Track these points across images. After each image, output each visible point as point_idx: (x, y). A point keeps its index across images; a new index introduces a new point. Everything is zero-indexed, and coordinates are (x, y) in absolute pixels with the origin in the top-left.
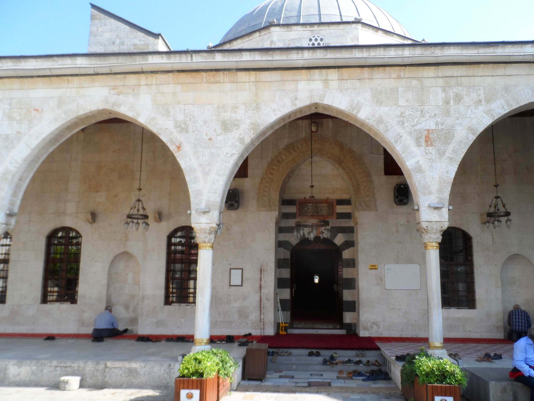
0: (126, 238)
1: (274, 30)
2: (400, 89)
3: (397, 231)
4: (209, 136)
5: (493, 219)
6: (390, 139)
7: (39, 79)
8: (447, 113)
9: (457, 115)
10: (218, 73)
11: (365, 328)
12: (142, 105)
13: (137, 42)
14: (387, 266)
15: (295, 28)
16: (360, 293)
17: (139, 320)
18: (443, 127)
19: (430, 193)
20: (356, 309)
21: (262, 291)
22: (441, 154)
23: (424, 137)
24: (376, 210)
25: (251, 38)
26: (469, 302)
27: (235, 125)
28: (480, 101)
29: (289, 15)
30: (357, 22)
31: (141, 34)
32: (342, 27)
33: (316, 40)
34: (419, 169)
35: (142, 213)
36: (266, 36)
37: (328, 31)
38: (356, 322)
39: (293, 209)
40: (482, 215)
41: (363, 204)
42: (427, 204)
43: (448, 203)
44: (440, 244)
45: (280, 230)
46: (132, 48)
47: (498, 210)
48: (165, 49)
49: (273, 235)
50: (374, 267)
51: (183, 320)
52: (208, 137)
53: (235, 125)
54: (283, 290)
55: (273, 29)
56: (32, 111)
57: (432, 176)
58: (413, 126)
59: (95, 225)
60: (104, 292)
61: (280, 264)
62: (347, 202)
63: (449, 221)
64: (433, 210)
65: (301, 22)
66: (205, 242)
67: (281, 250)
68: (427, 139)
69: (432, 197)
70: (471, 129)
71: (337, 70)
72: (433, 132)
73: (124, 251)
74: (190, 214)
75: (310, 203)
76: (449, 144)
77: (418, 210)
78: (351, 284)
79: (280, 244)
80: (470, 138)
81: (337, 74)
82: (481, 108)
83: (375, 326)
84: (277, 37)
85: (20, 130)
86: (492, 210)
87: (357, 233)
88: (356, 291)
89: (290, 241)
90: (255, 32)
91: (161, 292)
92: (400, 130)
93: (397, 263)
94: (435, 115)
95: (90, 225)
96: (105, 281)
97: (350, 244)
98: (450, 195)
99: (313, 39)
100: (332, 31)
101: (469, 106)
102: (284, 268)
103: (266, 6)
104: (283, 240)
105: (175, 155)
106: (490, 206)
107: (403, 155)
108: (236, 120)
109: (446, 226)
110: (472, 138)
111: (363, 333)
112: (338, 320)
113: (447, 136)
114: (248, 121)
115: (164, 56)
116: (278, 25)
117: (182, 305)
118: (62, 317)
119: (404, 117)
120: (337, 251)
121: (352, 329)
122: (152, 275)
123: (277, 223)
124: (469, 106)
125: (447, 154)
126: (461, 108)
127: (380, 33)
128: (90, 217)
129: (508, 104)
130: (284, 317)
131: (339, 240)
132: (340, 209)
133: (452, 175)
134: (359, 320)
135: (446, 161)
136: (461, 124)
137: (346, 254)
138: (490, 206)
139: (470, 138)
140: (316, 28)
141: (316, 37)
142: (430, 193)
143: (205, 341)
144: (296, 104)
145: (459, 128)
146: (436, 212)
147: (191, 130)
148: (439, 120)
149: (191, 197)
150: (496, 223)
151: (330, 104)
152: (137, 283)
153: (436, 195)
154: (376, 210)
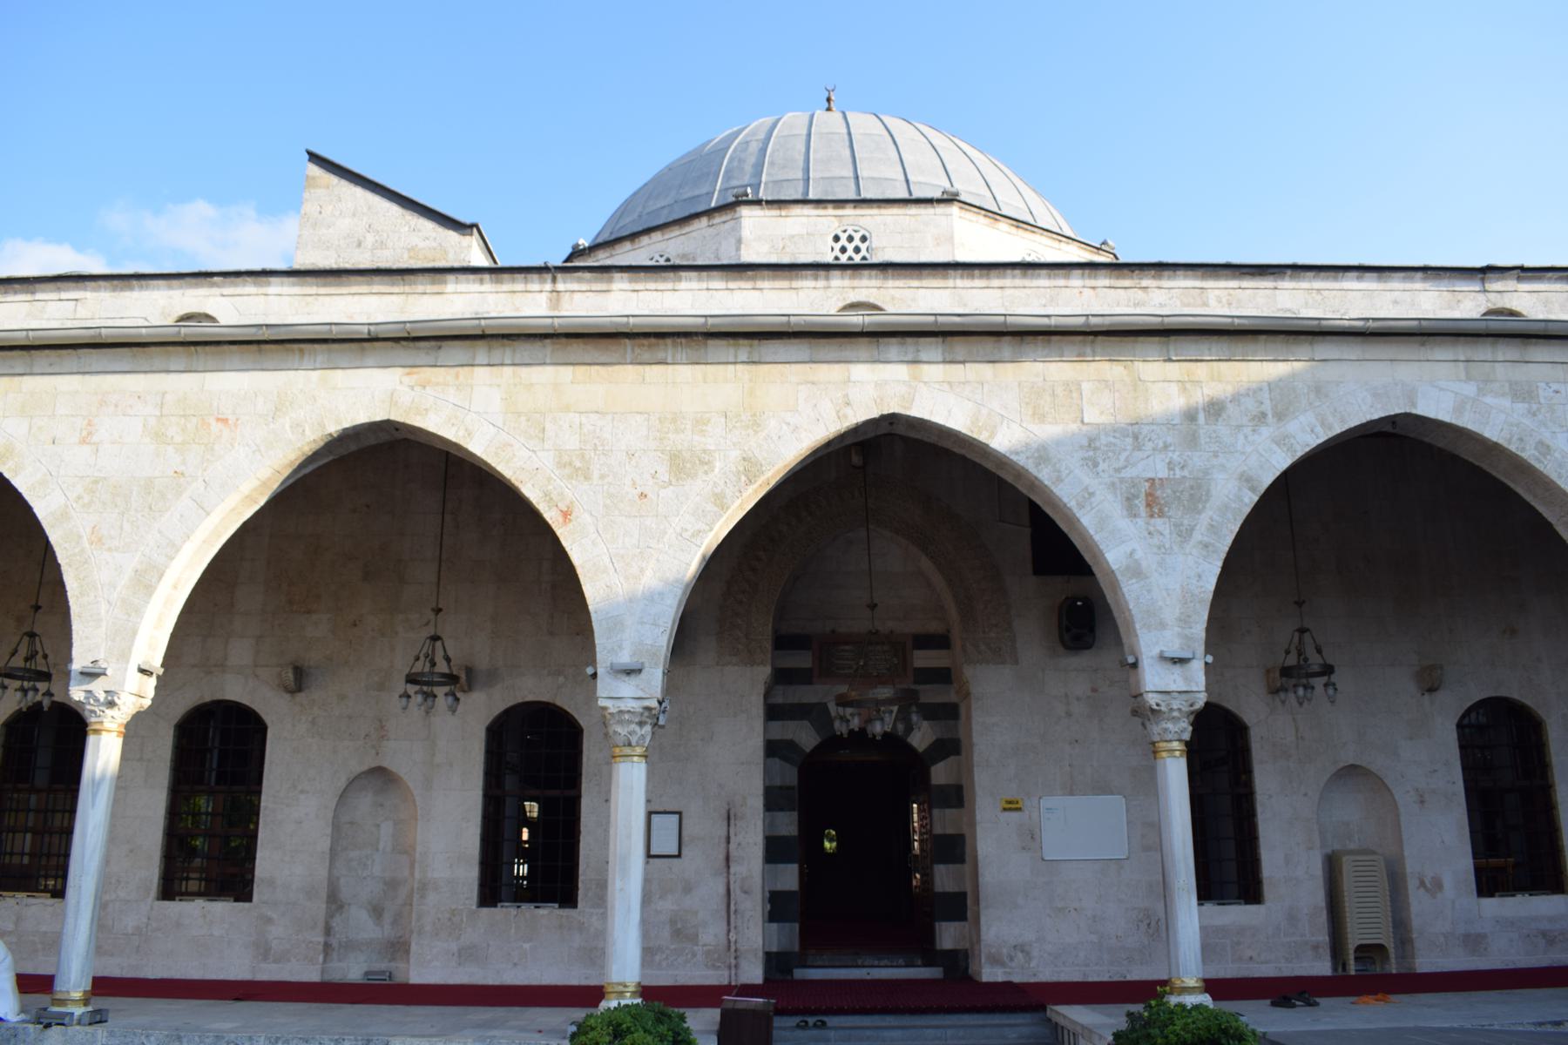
0: (381, 730)
1: (750, 217)
2: (1085, 386)
3: (1069, 714)
4: (643, 485)
5: (1293, 681)
6: (1065, 500)
7: (234, 348)
8: (1192, 441)
9: (1215, 447)
10: (661, 341)
11: (996, 961)
12: (466, 409)
13: (415, 240)
14: (1046, 802)
15: (797, 210)
16: (981, 871)
17: (414, 948)
18: (1186, 473)
19: (1163, 625)
20: (969, 914)
21: (732, 870)
22: (1184, 534)
23: (1143, 496)
24: (1016, 662)
25: (687, 229)
26: (1250, 891)
27: (702, 463)
28: (1264, 415)
29: (780, 177)
30: (949, 199)
31: (428, 226)
32: (913, 210)
33: (850, 239)
34: (1137, 572)
35: (446, 671)
36: (727, 226)
37: (878, 219)
38: (967, 946)
39: (802, 660)
40: (1268, 671)
41: (983, 647)
42: (1156, 651)
43: (1203, 648)
44: (1187, 744)
45: (773, 713)
46: (406, 256)
47: (1306, 660)
48: (484, 262)
49: (758, 724)
50: (1012, 806)
51: (527, 946)
52: (639, 490)
53: (702, 463)
54: (781, 866)
55: (745, 211)
56: (212, 421)
57: (1165, 586)
58: (1118, 470)
59: (300, 697)
60: (322, 873)
61: (774, 799)
62: (940, 641)
63: (1207, 690)
64: (1169, 665)
65: (811, 196)
66: (630, 745)
67: (777, 763)
68: (1152, 500)
69: (1168, 633)
70: (1247, 480)
71: (940, 340)
72: (1162, 485)
73: (373, 765)
74: (595, 675)
75: (846, 643)
76: (1199, 513)
77: (1135, 665)
78: (954, 849)
79: (773, 749)
80: (1246, 500)
81: (940, 351)
82: (1266, 431)
83: (1020, 955)
84: (760, 233)
85: (182, 468)
86: (1292, 660)
87: (969, 718)
88: (967, 867)
89: (796, 740)
90: (697, 216)
91: (470, 874)
92: (1087, 479)
93: (1072, 794)
94: (1166, 447)
95: (288, 696)
96: (325, 844)
97: (949, 747)
98: (1208, 630)
99: (844, 237)
100: (889, 219)
101: (1239, 427)
102: (782, 810)
103: (721, 150)
104: (778, 737)
105: (559, 532)
106: (1288, 652)
107: (1096, 538)
108: (704, 451)
109: (1201, 701)
110: (1251, 499)
111: (990, 974)
112: (922, 947)
113: (1195, 494)
114: (735, 454)
115: (487, 277)
116: (758, 202)
117: (525, 906)
118: (209, 937)
119: (1095, 449)
120: (918, 765)
121: (958, 963)
122: (447, 823)
123: (767, 695)
124: (1239, 427)
125: (1197, 536)
126: (1222, 429)
127: (1004, 226)
128: (290, 675)
129: (1323, 424)
130: (787, 936)
131: (921, 738)
132: (924, 659)
133: (1211, 584)
134: (979, 941)
135: (1194, 551)
136: (1223, 468)
137: (940, 774)
138: (1288, 652)
139: (1246, 500)
140: (849, 211)
141: (850, 232)
142: (1163, 625)
143: (631, 989)
144: (846, 416)
145: (1219, 477)
146: (1177, 669)
147: (596, 475)
148: (1175, 456)
149: (596, 635)
150: (1301, 691)
151: (926, 417)
152: (404, 849)
153: (1177, 629)
154: (1016, 662)
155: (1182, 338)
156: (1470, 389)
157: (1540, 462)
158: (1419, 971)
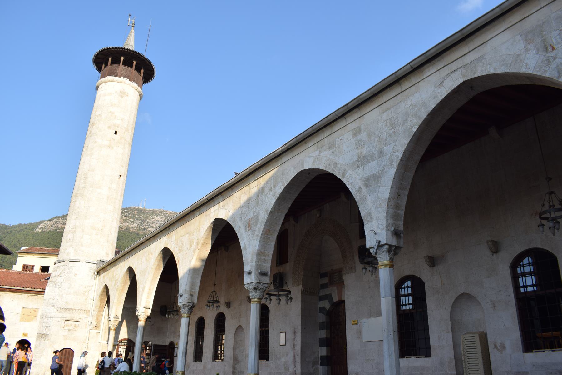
14: (363, 321)
93: (370, 317)
155: (383, 93)
156: (317, 153)
157: (334, 171)
158: (206, 257)
